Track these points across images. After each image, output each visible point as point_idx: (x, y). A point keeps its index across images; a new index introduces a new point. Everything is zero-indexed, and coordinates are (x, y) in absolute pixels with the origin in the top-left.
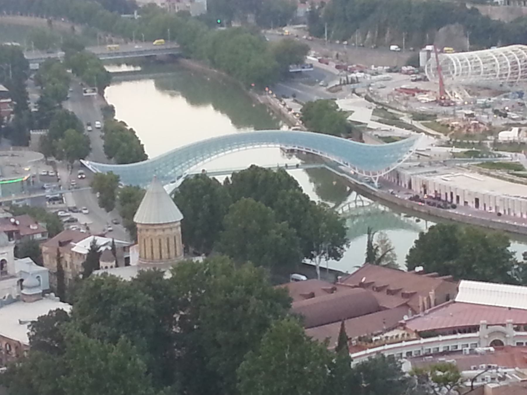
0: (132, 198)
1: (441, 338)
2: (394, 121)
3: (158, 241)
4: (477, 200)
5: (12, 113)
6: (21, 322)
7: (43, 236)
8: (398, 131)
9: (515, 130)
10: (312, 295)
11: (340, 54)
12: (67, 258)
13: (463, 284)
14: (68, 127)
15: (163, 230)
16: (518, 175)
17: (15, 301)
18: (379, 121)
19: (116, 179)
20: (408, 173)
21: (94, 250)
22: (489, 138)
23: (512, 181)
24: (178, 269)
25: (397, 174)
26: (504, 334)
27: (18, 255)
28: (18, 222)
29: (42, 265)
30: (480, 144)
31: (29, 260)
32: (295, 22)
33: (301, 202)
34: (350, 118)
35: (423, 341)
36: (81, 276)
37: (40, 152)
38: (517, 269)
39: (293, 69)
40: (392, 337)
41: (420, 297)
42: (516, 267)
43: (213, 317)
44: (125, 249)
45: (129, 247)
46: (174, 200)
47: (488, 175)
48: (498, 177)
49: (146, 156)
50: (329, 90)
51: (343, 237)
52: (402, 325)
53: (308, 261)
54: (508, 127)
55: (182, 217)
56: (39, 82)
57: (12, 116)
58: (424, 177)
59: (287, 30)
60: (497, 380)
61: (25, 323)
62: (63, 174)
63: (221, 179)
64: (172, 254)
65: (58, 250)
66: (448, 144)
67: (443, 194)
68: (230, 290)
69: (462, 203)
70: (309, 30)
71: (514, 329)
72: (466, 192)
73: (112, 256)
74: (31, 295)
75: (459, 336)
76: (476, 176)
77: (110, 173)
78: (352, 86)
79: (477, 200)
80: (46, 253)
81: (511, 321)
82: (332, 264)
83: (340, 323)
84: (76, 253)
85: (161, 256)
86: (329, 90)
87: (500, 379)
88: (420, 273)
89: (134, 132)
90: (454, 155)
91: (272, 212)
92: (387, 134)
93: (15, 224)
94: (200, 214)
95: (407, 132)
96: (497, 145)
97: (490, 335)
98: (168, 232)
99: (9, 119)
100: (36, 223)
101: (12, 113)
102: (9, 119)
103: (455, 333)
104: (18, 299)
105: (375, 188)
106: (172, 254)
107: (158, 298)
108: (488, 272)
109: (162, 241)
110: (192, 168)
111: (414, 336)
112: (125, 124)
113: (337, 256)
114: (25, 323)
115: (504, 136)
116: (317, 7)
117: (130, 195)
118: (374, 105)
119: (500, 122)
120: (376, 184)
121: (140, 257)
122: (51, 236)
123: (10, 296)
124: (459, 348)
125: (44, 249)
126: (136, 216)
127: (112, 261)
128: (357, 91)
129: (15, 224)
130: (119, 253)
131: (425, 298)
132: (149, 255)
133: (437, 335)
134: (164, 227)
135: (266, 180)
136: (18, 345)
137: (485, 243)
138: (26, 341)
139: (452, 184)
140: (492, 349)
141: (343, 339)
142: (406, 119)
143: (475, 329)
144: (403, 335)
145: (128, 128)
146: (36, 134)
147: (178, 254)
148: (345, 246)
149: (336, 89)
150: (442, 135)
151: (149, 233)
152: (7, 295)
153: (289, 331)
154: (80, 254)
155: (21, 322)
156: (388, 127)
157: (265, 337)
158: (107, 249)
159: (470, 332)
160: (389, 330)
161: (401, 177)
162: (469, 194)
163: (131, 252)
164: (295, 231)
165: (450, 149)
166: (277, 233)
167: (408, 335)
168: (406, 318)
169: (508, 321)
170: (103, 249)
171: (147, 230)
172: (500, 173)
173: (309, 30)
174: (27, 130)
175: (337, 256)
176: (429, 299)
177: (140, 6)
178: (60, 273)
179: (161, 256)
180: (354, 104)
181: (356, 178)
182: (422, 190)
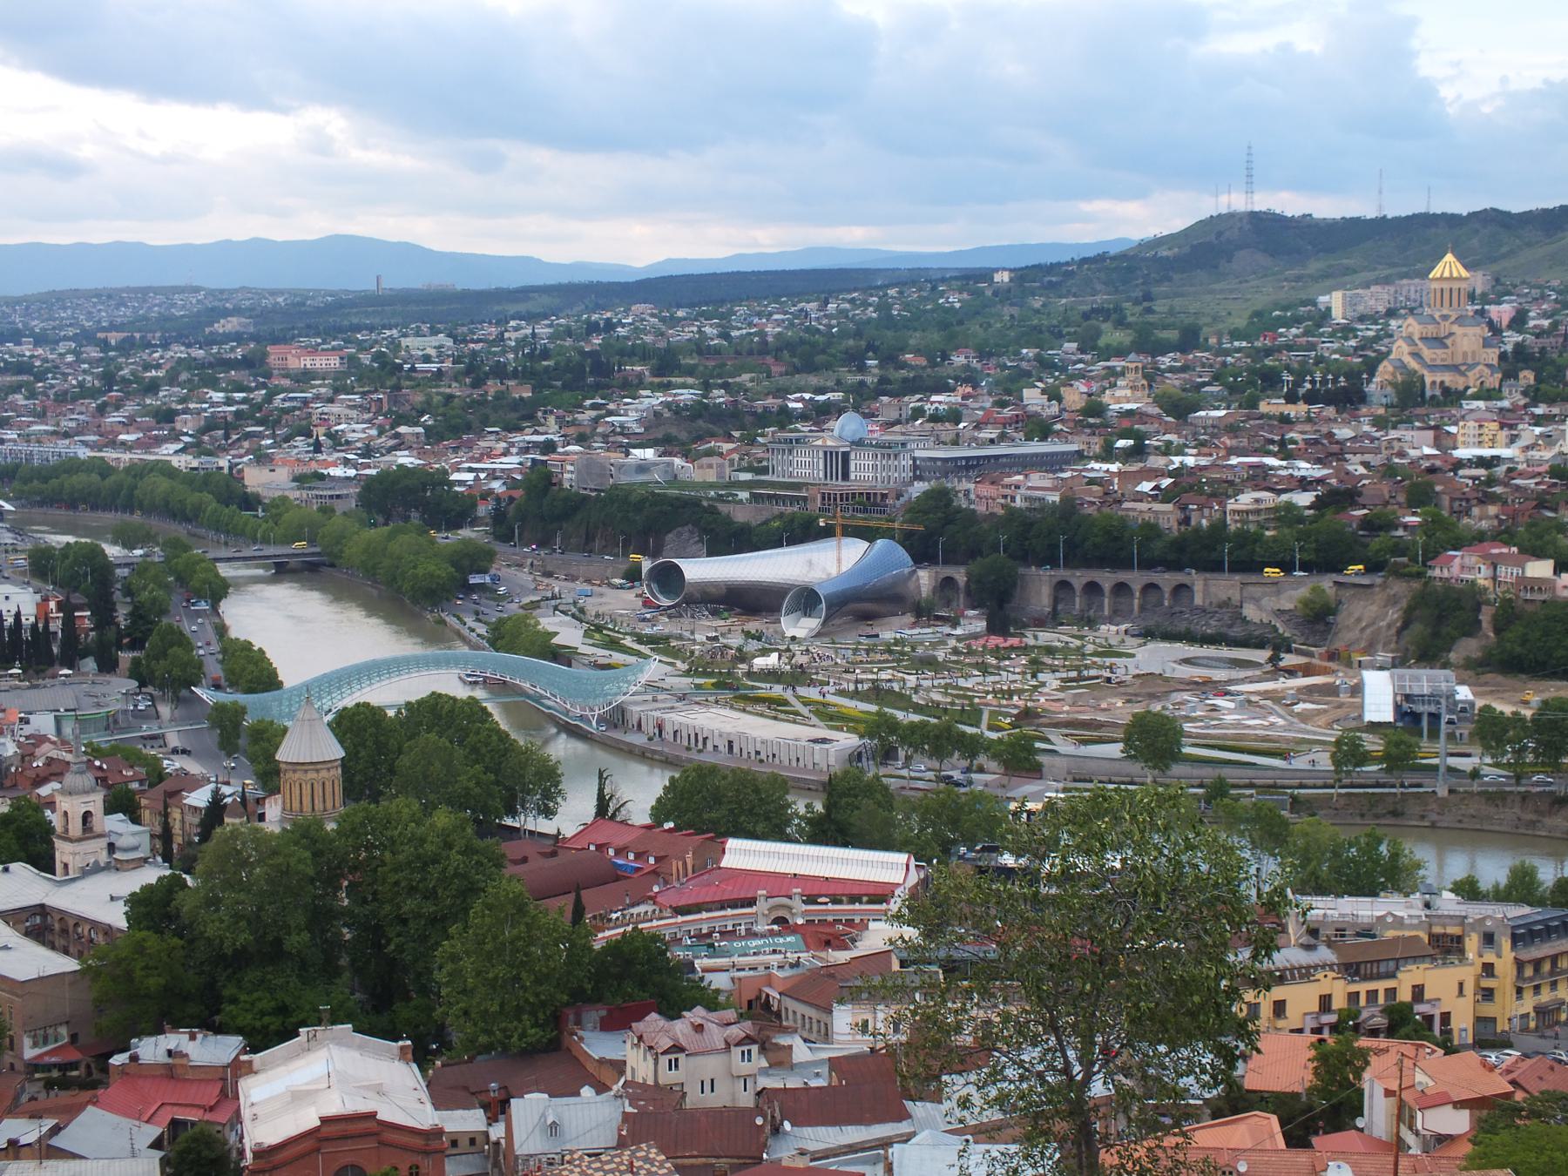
0: (265, 736)
1: (705, 915)
2: (614, 644)
3: (309, 786)
4: (730, 743)
5: (92, 630)
6: (112, 898)
7: (141, 785)
8: (618, 657)
9: (775, 655)
10: (525, 860)
11: (535, 562)
12: (176, 814)
13: (732, 843)
14: (171, 646)
15: (317, 771)
16: (782, 712)
17: (103, 869)
18: (593, 645)
19: (241, 711)
20: (639, 708)
21: (217, 798)
22: (740, 666)
23: (775, 718)
24: (341, 820)
25: (621, 710)
26: (790, 908)
27: (109, 810)
28: (105, 766)
29: (140, 824)
30: (729, 673)
31: (121, 816)
32: (474, 522)
33: (501, 740)
34: (555, 640)
35: (680, 919)
36: (196, 839)
37: (130, 677)
38: (799, 824)
39: (475, 579)
40: (639, 915)
41: (674, 863)
42: (796, 821)
43: (397, 883)
44: (259, 802)
45: (264, 798)
46: (333, 730)
47: (744, 711)
48: (757, 714)
49: (281, 683)
50: (522, 607)
51: (556, 786)
52: (651, 898)
53: (509, 822)
54: (764, 652)
55: (342, 754)
56: (128, 591)
57: (92, 634)
58: (657, 714)
59: (466, 533)
60: (787, 967)
61: (118, 898)
62: (165, 710)
63: (391, 713)
64: (329, 804)
65: (165, 802)
66: (687, 673)
67: (685, 735)
68: (423, 840)
69: (710, 747)
70: (493, 533)
71: (803, 902)
72: (716, 733)
73: (242, 810)
74: (127, 861)
75: (729, 912)
76: (727, 712)
77: (235, 703)
78: (553, 602)
79: (730, 743)
80: (145, 807)
81: (799, 890)
82: (545, 826)
83: (573, 895)
84: (190, 806)
85: (313, 809)
86: (522, 607)
87: (792, 966)
88: (670, 830)
89: (264, 653)
90: (698, 686)
91: (460, 753)
92: (606, 661)
93: (100, 768)
94: (363, 753)
95: (632, 659)
96: (750, 674)
97: (771, 909)
98: (324, 774)
99: (86, 638)
100: (132, 767)
101: (92, 630)
102: (86, 638)
103: (723, 908)
104: (107, 868)
105: (593, 727)
106: (329, 804)
107: (317, 854)
108: (760, 828)
109: (316, 785)
110: (354, 696)
111: (668, 913)
112: (250, 643)
113: (548, 813)
114: (118, 898)
115: (760, 662)
116: (503, 505)
117: (263, 731)
118: (586, 626)
119: (753, 646)
120: (594, 723)
121: (284, 809)
122: (151, 786)
123: (96, 862)
124: (730, 928)
125: (144, 802)
126: (280, 751)
127: (241, 817)
128: (560, 608)
129: (100, 768)
130: (251, 805)
131: (680, 863)
132: (296, 805)
133: (699, 912)
134: (319, 766)
135: (452, 711)
136: (108, 930)
137: (757, 791)
138: (122, 924)
139: (696, 723)
140: (775, 927)
141: (579, 912)
142: (628, 642)
143: (751, 902)
144: (654, 911)
145: (256, 648)
146: (125, 657)
147: (337, 805)
148: (559, 799)
149: (535, 605)
150: (679, 663)
151: (297, 775)
152: (92, 861)
153: (511, 895)
154: (196, 808)
155: (112, 898)
156: (607, 653)
157: (478, 905)
158: (235, 800)
159: (742, 906)
160: (633, 905)
161: (628, 716)
162: (720, 736)
163: (267, 805)
164: (492, 777)
165: (690, 680)
166: (469, 780)
167: (661, 911)
168: (656, 889)
169: (795, 890)
170: (228, 800)
171: (294, 771)
172: (759, 708)
173: (493, 533)
174: (113, 650)
175: (548, 813)
176: (685, 864)
177: (266, 501)
178: (166, 836)
179: (313, 809)
180: (561, 624)
181: (567, 715)
182: (657, 731)
